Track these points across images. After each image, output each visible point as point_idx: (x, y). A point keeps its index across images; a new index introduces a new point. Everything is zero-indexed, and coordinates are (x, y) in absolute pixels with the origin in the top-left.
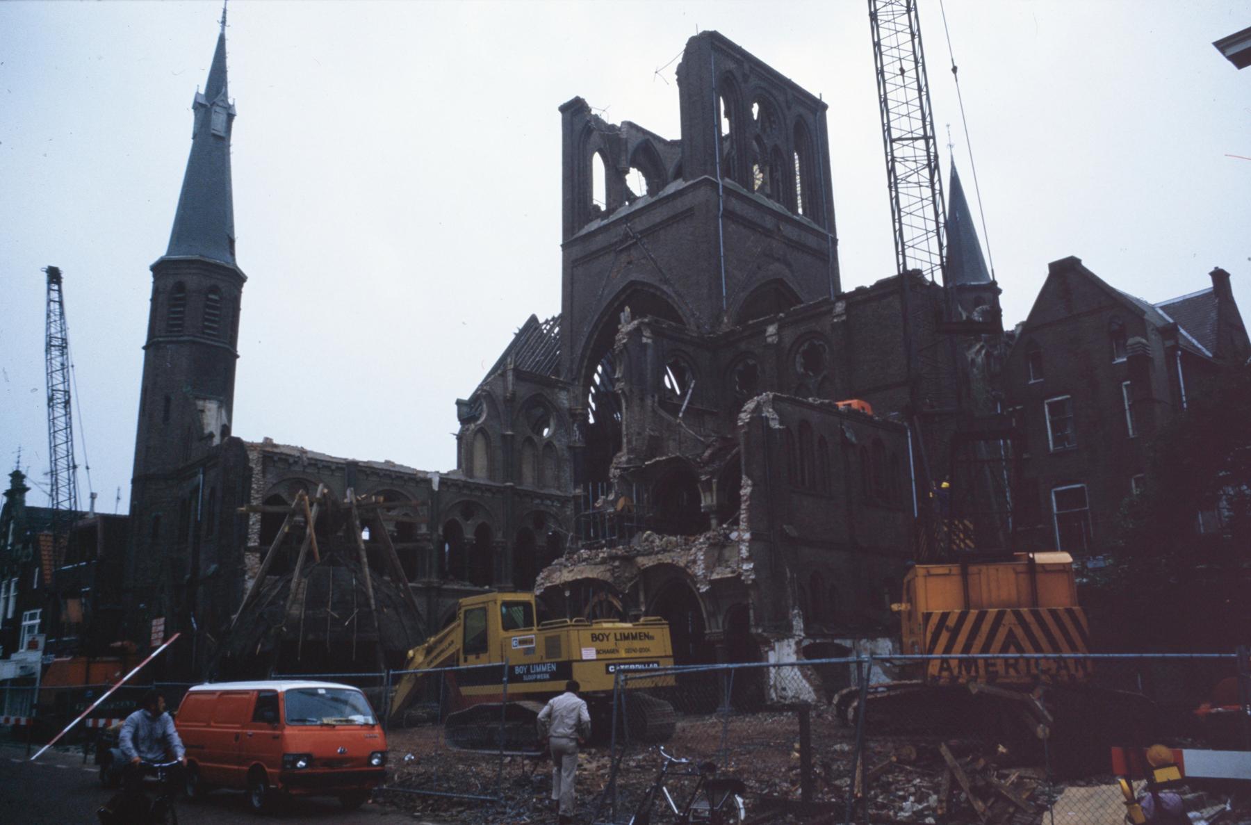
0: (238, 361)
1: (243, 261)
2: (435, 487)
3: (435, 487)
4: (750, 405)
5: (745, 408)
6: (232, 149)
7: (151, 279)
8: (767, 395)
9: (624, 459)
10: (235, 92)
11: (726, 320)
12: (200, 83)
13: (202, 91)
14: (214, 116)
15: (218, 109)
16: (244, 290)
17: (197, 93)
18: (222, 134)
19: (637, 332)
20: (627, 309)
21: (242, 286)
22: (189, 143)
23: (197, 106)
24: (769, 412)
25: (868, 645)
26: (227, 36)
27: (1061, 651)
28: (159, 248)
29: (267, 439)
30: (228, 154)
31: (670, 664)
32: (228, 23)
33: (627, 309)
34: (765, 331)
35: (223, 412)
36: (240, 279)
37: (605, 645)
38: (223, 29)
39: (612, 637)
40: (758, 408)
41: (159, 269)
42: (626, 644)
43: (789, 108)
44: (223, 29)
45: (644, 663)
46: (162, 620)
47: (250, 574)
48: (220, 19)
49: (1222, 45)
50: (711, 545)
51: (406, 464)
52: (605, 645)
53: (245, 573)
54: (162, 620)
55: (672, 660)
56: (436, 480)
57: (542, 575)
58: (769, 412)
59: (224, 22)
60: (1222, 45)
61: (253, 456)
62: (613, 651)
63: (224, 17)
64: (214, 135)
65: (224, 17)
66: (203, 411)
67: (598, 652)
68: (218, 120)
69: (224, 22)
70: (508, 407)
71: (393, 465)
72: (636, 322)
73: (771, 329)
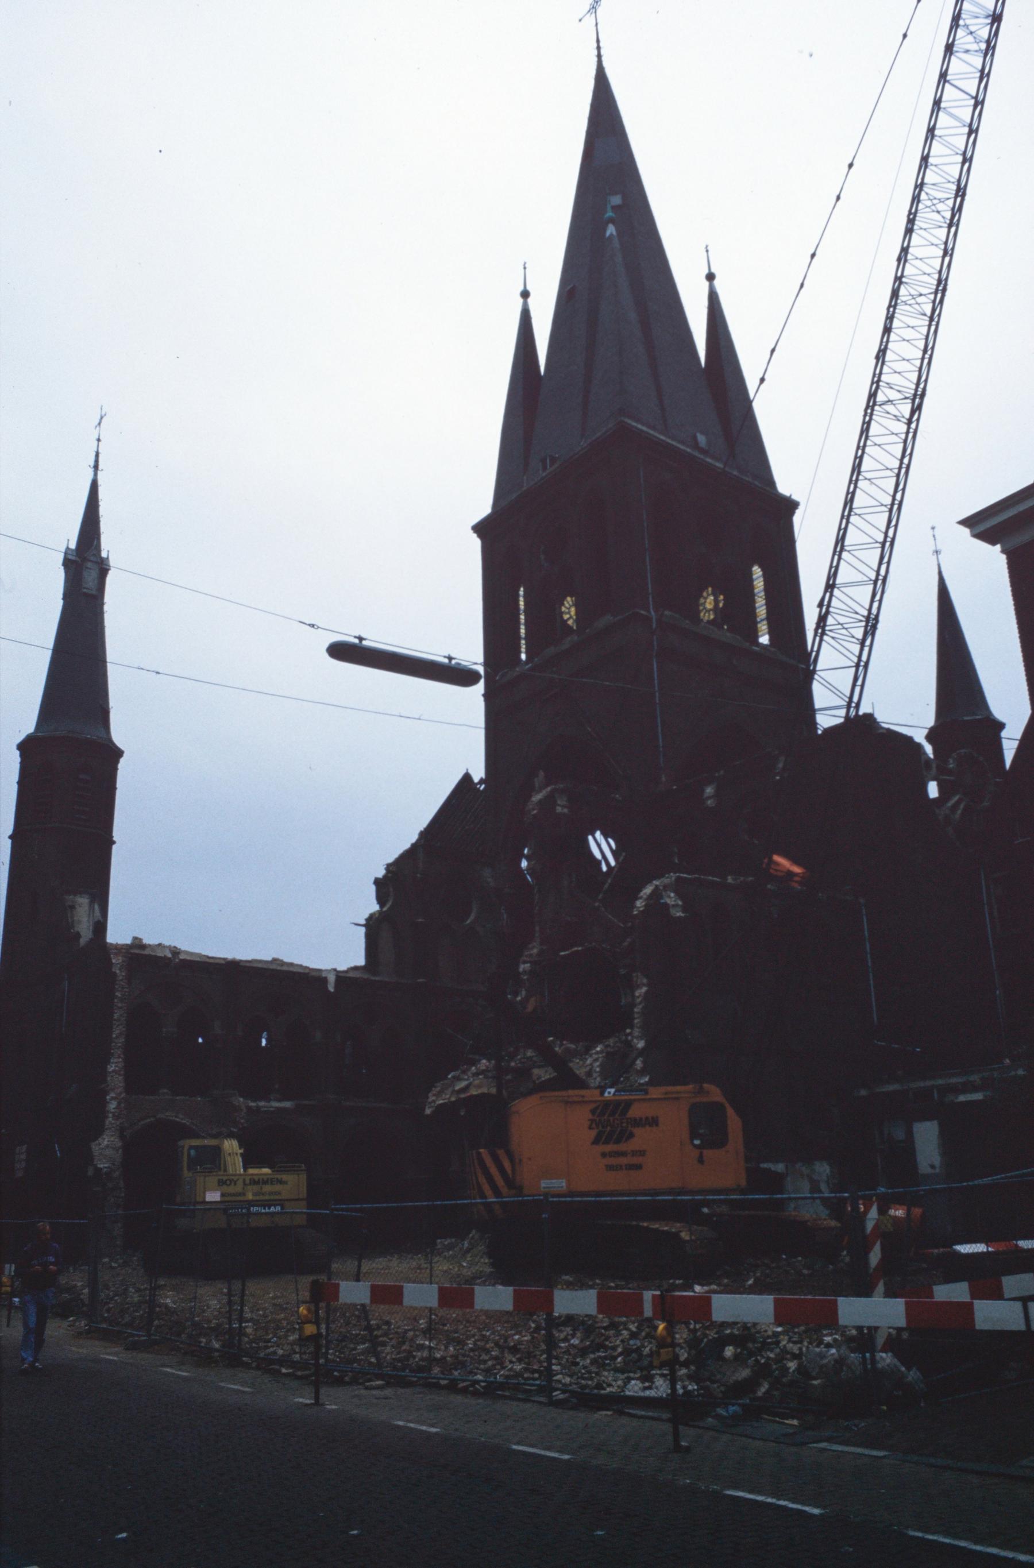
0: (114, 847)
1: (120, 733)
2: (331, 988)
3: (331, 988)
4: (648, 890)
5: (642, 894)
6: (106, 608)
7: (19, 759)
8: (671, 878)
9: (535, 951)
10: (109, 544)
11: (664, 779)
12: (71, 536)
13: (73, 546)
14: (85, 574)
15: (89, 565)
16: (120, 766)
17: (68, 548)
18: (94, 592)
19: (550, 800)
20: (542, 773)
21: (118, 762)
22: (60, 603)
23: (67, 563)
24: (671, 899)
25: (805, 1170)
26: (100, 482)
27: (486, 1198)
28: (28, 725)
29: (135, 938)
30: (101, 613)
31: (302, 1208)
32: (100, 467)
33: (542, 773)
34: (703, 791)
35: (96, 907)
36: (117, 754)
37: (231, 1189)
38: (96, 474)
39: (240, 1183)
40: (656, 894)
41: (26, 747)
42: (256, 1188)
44: (96, 474)
45: (651, 1195)
46: (25, 1147)
47: (112, 1095)
48: (92, 464)
49: (966, 522)
50: (608, 1053)
51: (296, 961)
52: (231, 1189)
53: (106, 1093)
54: (25, 1147)
55: (305, 1203)
56: (332, 978)
57: (435, 1091)
58: (671, 899)
59: (96, 467)
60: (966, 522)
61: (116, 960)
62: (239, 1194)
63: (97, 461)
64: (85, 594)
65: (97, 461)
66: (72, 907)
67: (223, 1195)
68: (90, 578)
69: (96, 467)
70: (418, 889)
71: (282, 963)
72: (549, 789)
73: (709, 790)
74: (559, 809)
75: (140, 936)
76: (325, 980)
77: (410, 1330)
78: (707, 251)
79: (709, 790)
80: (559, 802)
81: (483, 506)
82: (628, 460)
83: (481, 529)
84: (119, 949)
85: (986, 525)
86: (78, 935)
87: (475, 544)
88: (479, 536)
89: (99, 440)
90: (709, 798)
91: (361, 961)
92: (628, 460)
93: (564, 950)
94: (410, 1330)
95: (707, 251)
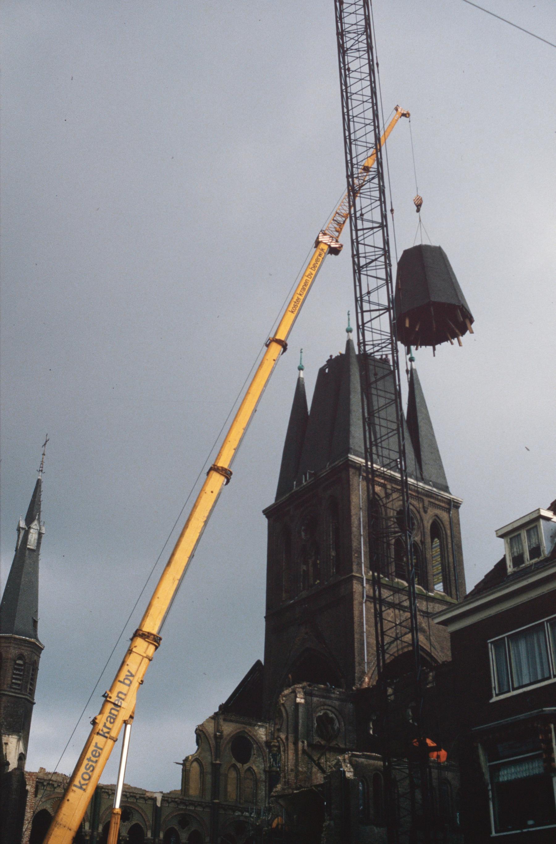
14: (30, 536)
29: (41, 768)
43: (426, 512)
56: (159, 798)
64: (29, 549)
74: (298, 700)
75: (44, 767)
76: (154, 800)
77: (423, 504)
78: (349, 315)
79: (390, 691)
80: (298, 696)
81: (270, 499)
82: (346, 478)
84: (31, 774)
85: (549, 509)
86: (8, 764)
87: (264, 521)
88: (267, 517)
90: (390, 695)
91: (178, 787)
92: (346, 478)
93: (297, 790)
94: (423, 504)
95: (349, 315)
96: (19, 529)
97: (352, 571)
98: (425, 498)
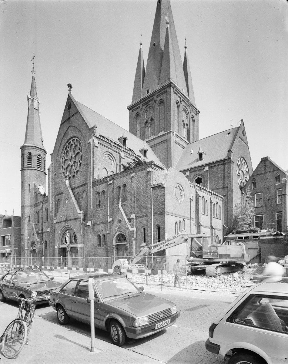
43: (190, 113)
81: (129, 102)
83: (130, 108)
89: (33, 64)
96: (28, 99)
97: (171, 129)
98: (191, 107)
